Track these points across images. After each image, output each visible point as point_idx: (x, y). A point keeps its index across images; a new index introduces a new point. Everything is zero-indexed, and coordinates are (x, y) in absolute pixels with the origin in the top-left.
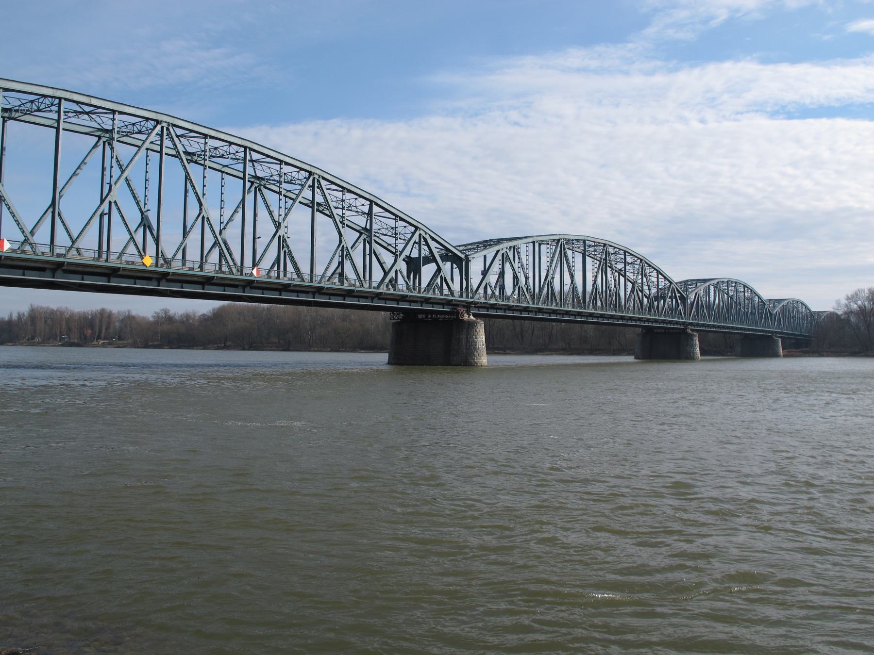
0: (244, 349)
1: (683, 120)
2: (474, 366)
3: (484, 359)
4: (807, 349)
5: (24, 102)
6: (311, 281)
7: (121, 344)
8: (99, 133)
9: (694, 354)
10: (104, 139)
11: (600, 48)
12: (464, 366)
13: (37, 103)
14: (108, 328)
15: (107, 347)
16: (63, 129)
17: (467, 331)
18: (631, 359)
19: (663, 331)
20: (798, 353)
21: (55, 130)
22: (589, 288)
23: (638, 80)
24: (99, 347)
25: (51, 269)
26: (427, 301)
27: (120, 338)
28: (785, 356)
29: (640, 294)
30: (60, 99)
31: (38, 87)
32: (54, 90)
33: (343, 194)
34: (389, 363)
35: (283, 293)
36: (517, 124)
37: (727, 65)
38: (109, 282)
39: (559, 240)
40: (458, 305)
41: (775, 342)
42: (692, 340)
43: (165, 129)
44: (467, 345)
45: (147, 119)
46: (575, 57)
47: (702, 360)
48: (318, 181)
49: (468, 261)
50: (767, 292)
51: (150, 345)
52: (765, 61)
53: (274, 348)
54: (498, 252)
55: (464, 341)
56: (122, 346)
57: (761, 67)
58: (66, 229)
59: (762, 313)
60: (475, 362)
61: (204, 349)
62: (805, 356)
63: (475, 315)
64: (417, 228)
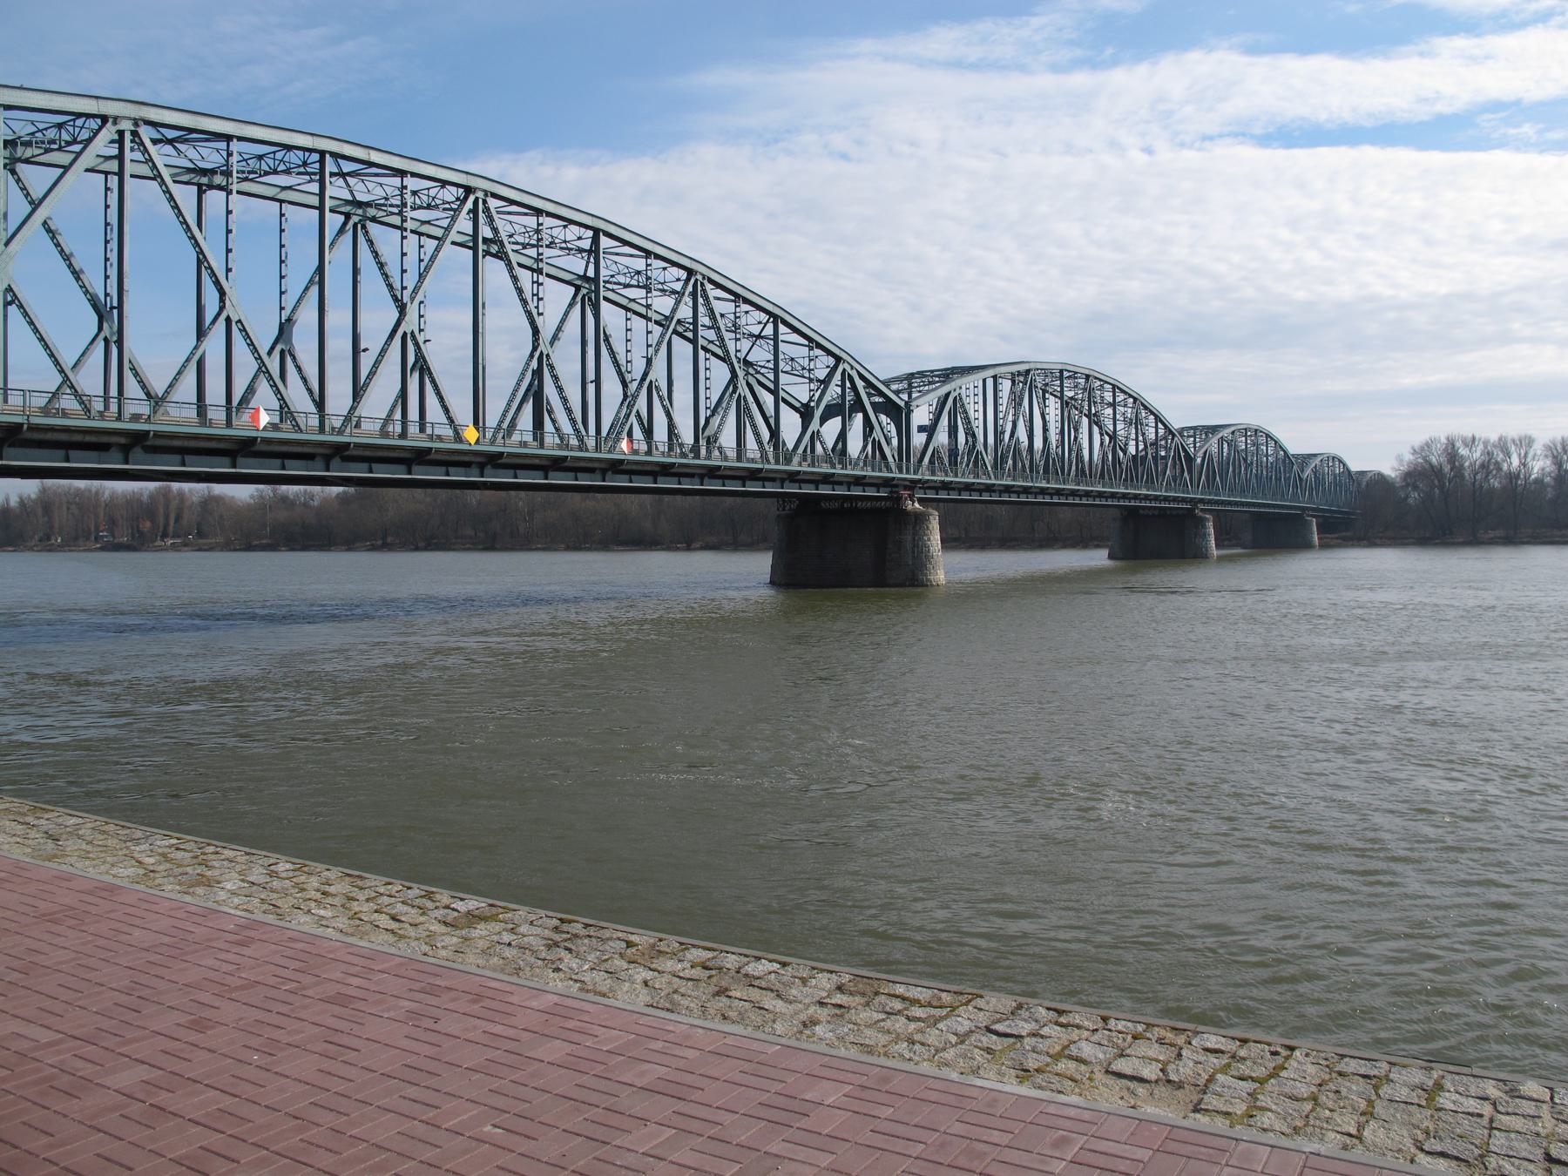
0: (417, 549)
1: (1115, 146)
2: (927, 586)
3: (1215, 552)
4: (1348, 534)
5: (41, 126)
6: (739, 458)
7: (204, 544)
8: (347, 209)
9: (1207, 550)
10: (355, 219)
11: (985, 26)
12: (909, 586)
13: (71, 129)
14: (177, 519)
15: (179, 551)
16: (132, 176)
17: (914, 527)
18: (1098, 558)
19: (1156, 512)
20: (1336, 541)
21: (317, 212)
22: (1038, 443)
23: (1046, 81)
24: (166, 550)
25: (323, 455)
26: (827, 479)
27: (200, 534)
28: (1325, 546)
29: (768, 399)
30: (322, 153)
31: (47, 96)
32: (101, 101)
33: (736, 307)
34: (772, 583)
35: (660, 479)
36: (845, 157)
37: (1194, 56)
38: (410, 473)
39: (1028, 372)
40: (896, 486)
41: (1307, 525)
42: (1204, 527)
43: (480, 202)
44: (913, 552)
45: (444, 183)
46: (943, 40)
47: (1221, 559)
48: (702, 284)
49: (909, 412)
50: (1297, 441)
51: (256, 546)
52: (1252, 50)
53: (467, 546)
54: (948, 395)
55: (909, 546)
56: (206, 547)
57: (1246, 59)
58: (41, 339)
59: (1290, 477)
60: (928, 580)
61: (349, 550)
62: (1346, 546)
63: (921, 501)
64: (838, 359)
